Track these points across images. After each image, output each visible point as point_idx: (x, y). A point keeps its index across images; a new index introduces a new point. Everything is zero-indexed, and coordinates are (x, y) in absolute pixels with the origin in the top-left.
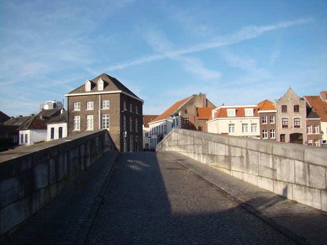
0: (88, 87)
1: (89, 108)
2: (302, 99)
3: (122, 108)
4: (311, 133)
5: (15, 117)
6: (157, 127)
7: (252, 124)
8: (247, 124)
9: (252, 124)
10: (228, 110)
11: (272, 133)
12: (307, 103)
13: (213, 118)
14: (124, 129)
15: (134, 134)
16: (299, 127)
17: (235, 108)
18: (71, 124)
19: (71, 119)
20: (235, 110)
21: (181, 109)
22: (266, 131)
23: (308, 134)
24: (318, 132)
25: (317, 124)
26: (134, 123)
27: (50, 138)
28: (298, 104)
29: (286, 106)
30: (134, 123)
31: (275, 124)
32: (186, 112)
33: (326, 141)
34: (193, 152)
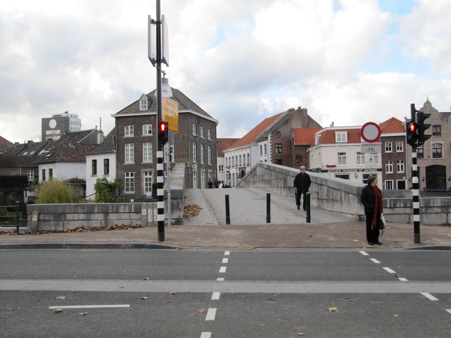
11: (400, 164)
13: (316, 144)
15: (207, 167)
26: (205, 152)
27: (103, 174)
30: (205, 152)
31: (404, 153)
34: (276, 186)
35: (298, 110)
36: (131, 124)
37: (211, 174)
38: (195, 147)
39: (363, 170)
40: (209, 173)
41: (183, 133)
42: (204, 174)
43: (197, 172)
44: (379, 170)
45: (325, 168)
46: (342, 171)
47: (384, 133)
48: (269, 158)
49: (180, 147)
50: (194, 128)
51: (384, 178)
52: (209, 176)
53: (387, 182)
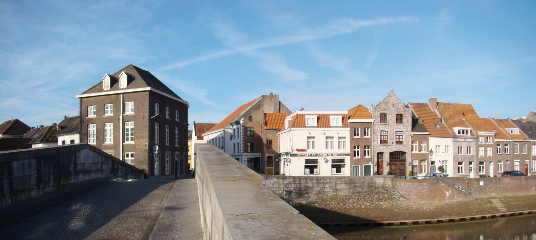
0: (107, 81)
1: (107, 113)
2: (407, 106)
3: (151, 111)
4: (417, 152)
5: (36, 127)
6: (213, 139)
7: (339, 138)
8: (332, 138)
9: (339, 138)
10: (306, 117)
12: (412, 112)
13: (286, 127)
14: (156, 142)
15: (173, 149)
16: (401, 143)
17: (316, 114)
18: (84, 135)
19: (84, 128)
20: (316, 117)
21: (244, 116)
22: (368, 148)
23: (413, 152)
24: (425, 150)
25: (424, 140)
26: (172, 133)
28: (401, 112)
29: (385, 115)
30: (172, 133)
31: (371, 138)
32: (250, 118)
33: (434, 162)
35: (270, 95)
36: (93, 104)
37: (179, 156)
38: (178, 132)
39: (332, 155)
40: (177, 155)
41: (143, 113)
42: (170, 156)
43: (160, 154)
44: (347, 155)
45: (296, 152)
46: (311, 155)
47: (353, 118)
48: (241, 141)
49: (140, 128)
50: (177, 114)
51: (352, 163)
52: (177, 158)
53: (354, 166)
